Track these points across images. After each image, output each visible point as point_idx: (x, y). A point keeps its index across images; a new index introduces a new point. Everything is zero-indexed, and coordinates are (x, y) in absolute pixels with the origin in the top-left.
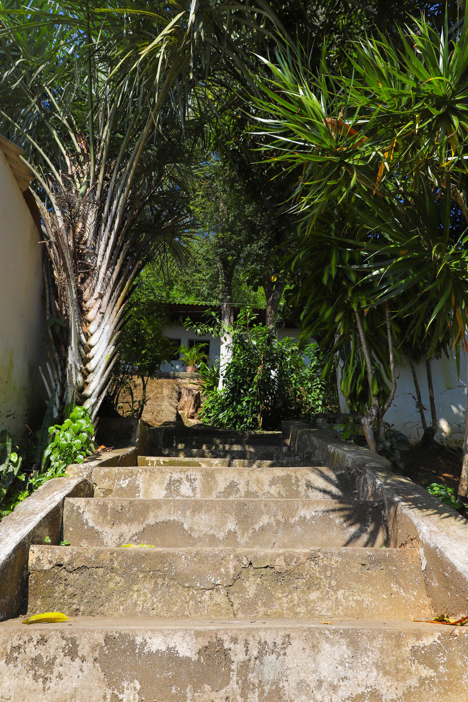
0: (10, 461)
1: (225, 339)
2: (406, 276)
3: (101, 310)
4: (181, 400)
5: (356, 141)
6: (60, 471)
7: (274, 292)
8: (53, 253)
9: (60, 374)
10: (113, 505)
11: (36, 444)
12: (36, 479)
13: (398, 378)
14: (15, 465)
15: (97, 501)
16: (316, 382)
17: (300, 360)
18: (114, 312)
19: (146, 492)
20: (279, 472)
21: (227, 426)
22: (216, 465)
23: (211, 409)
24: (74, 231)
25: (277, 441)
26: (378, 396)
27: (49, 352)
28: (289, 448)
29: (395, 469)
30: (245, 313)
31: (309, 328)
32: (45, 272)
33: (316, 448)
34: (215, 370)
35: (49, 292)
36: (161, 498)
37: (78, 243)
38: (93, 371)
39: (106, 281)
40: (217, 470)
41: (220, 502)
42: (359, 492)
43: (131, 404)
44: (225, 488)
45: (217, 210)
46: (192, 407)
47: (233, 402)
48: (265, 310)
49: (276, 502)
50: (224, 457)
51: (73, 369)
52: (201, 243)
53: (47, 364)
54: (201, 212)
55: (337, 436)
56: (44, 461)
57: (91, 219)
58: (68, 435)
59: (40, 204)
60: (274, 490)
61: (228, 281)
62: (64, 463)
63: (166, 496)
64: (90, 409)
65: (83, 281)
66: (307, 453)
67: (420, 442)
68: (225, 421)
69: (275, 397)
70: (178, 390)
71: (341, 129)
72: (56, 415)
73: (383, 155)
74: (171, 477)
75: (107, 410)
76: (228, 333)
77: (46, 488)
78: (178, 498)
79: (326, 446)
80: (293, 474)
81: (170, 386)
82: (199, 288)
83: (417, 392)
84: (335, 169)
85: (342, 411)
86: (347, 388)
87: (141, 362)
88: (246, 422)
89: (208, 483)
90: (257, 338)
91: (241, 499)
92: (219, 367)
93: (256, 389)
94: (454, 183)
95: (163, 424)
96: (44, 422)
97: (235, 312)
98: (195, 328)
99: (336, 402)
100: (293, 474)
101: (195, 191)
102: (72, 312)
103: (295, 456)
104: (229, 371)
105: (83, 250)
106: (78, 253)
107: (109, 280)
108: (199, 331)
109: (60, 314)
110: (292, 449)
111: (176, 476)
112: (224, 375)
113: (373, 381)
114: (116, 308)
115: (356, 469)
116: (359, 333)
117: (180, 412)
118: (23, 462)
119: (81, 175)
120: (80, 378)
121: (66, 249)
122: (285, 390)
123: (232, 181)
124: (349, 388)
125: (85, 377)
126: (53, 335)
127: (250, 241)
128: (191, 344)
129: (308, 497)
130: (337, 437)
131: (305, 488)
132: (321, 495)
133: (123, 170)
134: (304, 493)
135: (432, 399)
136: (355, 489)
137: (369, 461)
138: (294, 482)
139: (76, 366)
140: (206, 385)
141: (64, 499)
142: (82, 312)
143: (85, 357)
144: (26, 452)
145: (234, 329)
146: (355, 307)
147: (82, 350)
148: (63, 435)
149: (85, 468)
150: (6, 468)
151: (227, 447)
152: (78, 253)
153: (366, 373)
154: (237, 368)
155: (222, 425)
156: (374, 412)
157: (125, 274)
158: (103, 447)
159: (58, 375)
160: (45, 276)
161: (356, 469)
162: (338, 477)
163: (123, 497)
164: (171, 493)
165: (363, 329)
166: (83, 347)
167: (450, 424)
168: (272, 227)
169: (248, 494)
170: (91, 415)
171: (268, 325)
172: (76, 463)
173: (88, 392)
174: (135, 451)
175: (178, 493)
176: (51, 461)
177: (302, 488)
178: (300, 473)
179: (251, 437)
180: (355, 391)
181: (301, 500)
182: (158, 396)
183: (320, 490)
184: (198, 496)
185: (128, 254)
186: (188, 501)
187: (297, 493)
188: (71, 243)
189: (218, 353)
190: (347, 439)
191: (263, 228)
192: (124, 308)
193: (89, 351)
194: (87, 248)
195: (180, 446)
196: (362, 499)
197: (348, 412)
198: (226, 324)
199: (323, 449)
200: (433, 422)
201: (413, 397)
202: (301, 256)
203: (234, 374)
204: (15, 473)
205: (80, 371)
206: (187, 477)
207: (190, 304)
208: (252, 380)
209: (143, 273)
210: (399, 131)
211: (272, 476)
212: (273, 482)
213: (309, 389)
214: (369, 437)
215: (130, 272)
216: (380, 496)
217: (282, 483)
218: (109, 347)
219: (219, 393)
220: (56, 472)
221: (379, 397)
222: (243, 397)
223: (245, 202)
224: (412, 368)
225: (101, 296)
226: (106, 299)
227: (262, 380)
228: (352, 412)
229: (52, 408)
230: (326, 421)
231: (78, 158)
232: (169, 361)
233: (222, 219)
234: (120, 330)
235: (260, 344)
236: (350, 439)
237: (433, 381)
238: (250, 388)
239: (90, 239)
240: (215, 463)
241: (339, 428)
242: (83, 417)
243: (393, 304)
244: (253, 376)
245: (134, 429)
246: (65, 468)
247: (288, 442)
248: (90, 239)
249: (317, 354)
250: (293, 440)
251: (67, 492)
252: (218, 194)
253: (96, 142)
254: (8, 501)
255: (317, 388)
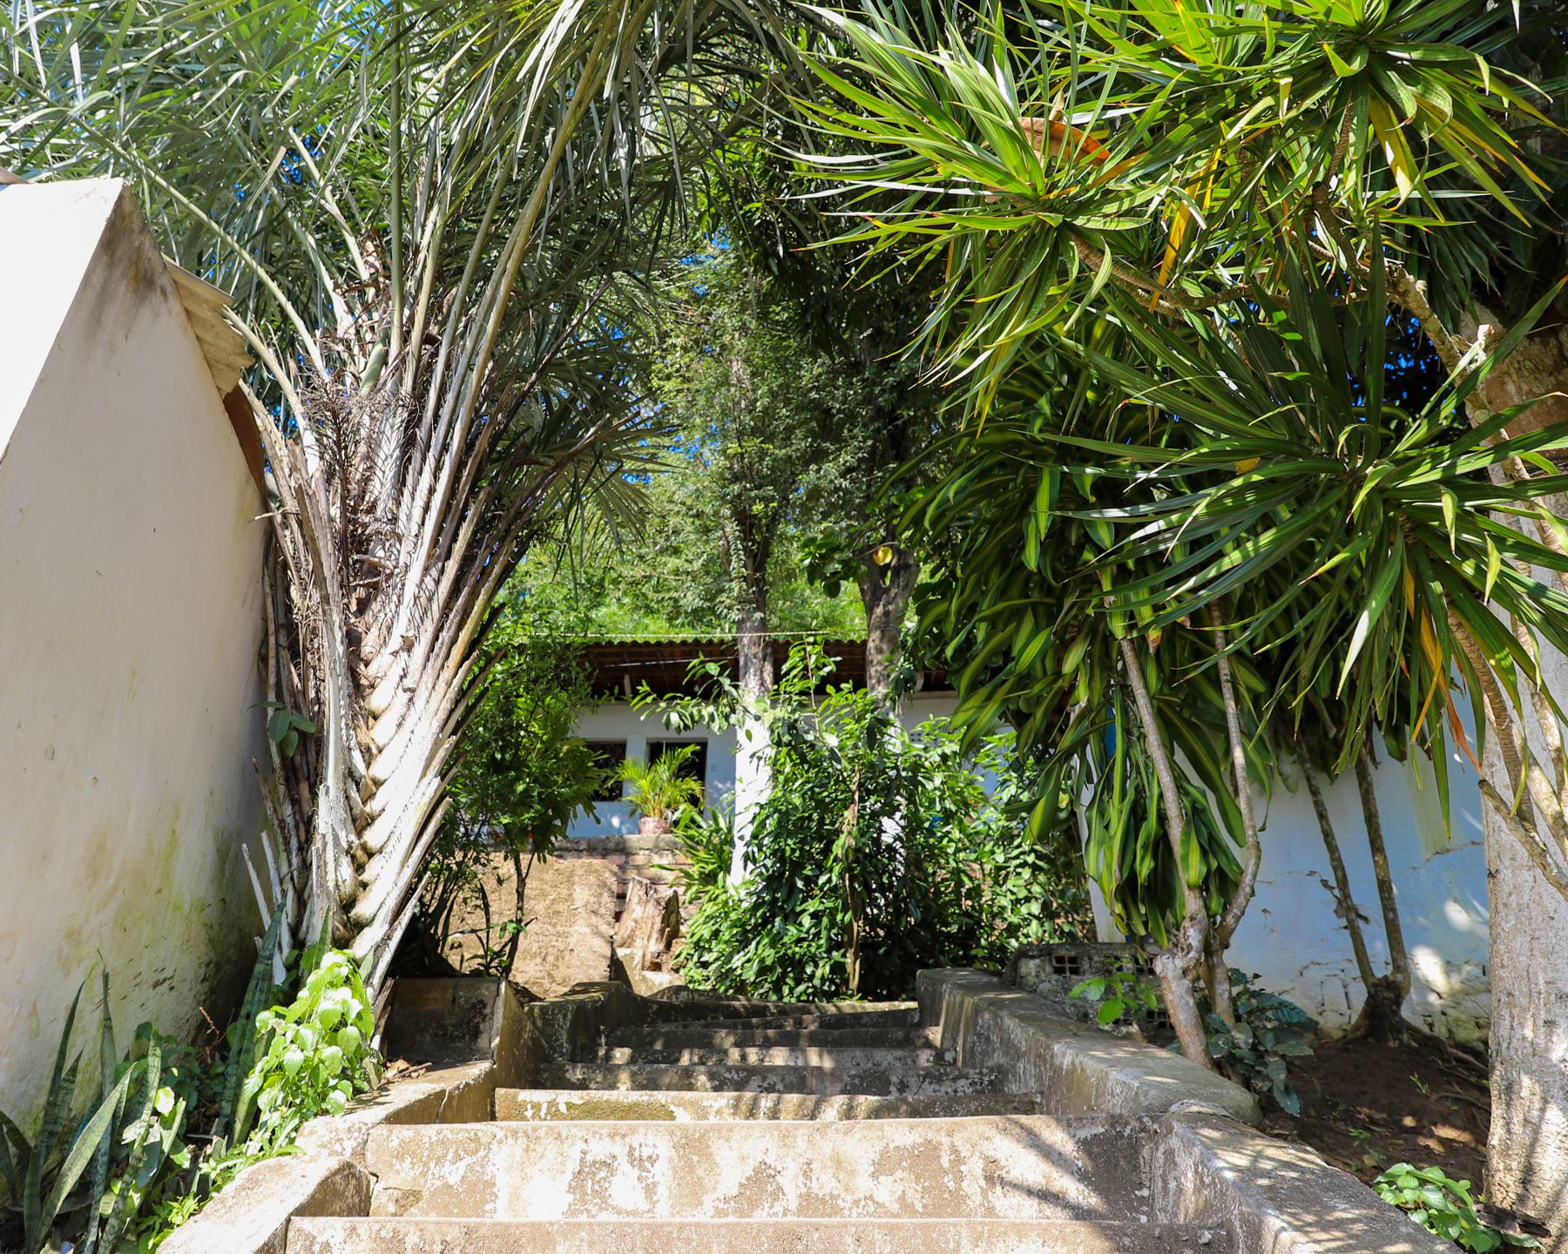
0: (155, 1113)
1: (749, 735)
2: (1267, 522)
3: (408, 683)
4: (624, 916)
5: (1105, 170)
6: (281, 1140)
7: (887, 590)
8: (290, 540)
9: (295, 861)
10: (421, 1237)
11: (224, 1059)
12: (218, 1162)
13: (1263, 829)
14: (166, 1123)
15: (376, 1227)
16: (1019, 846)
17: (971, 783)
18: (441, 686)
19: (515, 1197)
20: (903, 1132)
21: (756, 989)
22: (718, 1112)
23: (709, 941)
24: (345, 481)
25: (904, 1033)
26: (1203, 887)
27: (269, 804)
28: (939, 1055)
29: (1267, 1118)
30: (803, 659)
31: (983, 692)
32: (268, 590)
33: (1019, 1055)
34: (723, 824)
35: (280, 639)
36: (556, 1216)
37: (355, 511)
38: (380, 851)
39: (422, 603)
40: (718, 1129)
41: (723, 1231)
42: (1152, 1196)
43: (483, 935)
44: (741, 1185)
45: (724, 381)
46: (655, 936)
47: (774, 916)
48: (865, 643)
49: (891, 1230)
50: (740, 1086)
51: (330, 847)
52: (682, 476)
53: (264, 836)
54: (679, 391)
55: (1086, 1015)
56: (242, 1109)
57: (390, 447)
58: (308, 1033)
59: (263, 419)
60: (886, 1191)
61: (756, 571)
62: (295, 1113)
63: (571, 1211)
64: (370, 957)
65: (363, 606)
66: (991, 1070)
67: (1356, 1028)
68: (750, 976)
69: (896, 895)
70: (615, 888)
71: (1060, 140)
72: (280, 976)
73: (1176, 198)
74: (584, 1153)
75: (418, 955)
76: (757, 718)
77: (243, 1188)
78: (604, 1217)
79: (1048, 1047)
80: (945, 1140)
81: (592, 879)
82: (675, 595)
83: (1335, 868)
84: (1047, 243)
85: (1102, 936)
86: (1109, 867)
87: (513, 814)
88: (812, 977)
89: (691, 1168)
90: (838, 726)
91: (789, 1218)
92: (733, 813)
93: (841, 876)
94: (1393, 254)
95: (573, 992)
96: (248, 997)
97: (777, 653)
98: (664, 711)
99: (1079, 905)
100: (945, 1140)
101: (663, 336)
102: (333, 691)
103: (955, 1080)
104: (763, 825)
105: (365, 526)
106: (353, 536)
107: (430, 600)
108: (674, 718)
109: (301, 699)
110: (949, 1057)
111: (600, 1149)
112: (748, 838)
113: (1186, 841)
114: (447, 674)
115: (1140, 1119)
116: (1134, 702)
117: (621, 952)
118: (187, 1112)
119: (368, 337)
120: (346, 871)
121: (324, 528)
122: (927, 875)
123: (765, 300)
124: (1115, 867)
125: (359, 868)
126: (284, 760)
127: (818, 456)
128: (655, 751)
129: (990, 1211)
130: (1084, 1017)
131: (983, 1183)
132: (1031, 1205)
133: (473, 310)
134: (978, 1199)
135: (1384, 886)
136: (1141, 1186)
137: (1179, 1096)
138: (946, 1165)
139: (336, 838)
140: (695, 871)
141: (288, 1221)
142: (358, 690)
143: (362, 812)
144: (197, 1083)
145: (773, 706)
146: (1118, 627)
147: (354, 794)
148: (289, 1038)
149: (349, 1130)
150: (142, 1131)
151: (753, 1055)
152: (353, 536)
153: (1162, 818)
154: (785, 816)
155: (741, 987)
156: (1193, 936)
157: (471, 580)
158: (401, 1064)
159: (290, 865)
160: (269, 601)
161: (1140, 1119)
162: (1085, 1145)
163: (450, 1214)
164: (584, 1202)
165: (1146, 687)
166: (357, 784)
167: (1450, 967)
168: (879, 412)
169: (809, 1202)
170: (370, 976)
171: (873, 689)
172: (325, 1112)
173: (362, 909)
174: (490, 1074)
175: (604, 1200)
176: (259, 1111)
177: (973, 1186)
178: (966, 1134)
179: (827, 1023)
180: (1133, 875)
181: (968, 1224)
182: (560, 907)
183: (1030, 1192)
184: (663, 1212)
185: (483, 526)
186: (629, 1225)
187: (955, 1202)
188: (335, 512)
189: (730, 776)
190: (1117, 1022)
191: (851, 417)
192: (470, 669)
193: (372, 796)
194: (376, 520)
195: (621, 1055)
196: (1163, 1219)
197: (1120, 937)
198: (750, 692)
199: (1039, 1056)
200: (1394, 960)
201: (1325, 883)
202: (951, 495)
203: (776, 836)
204: (166, 1147)
205: (347, 852)
206: (631, 1154)
207: (653, 642)
208: (826, 851)
209: (523, 565)
210: (1231, 126)
211: (879, 1146)
212: (882, 1167)
213: (999, 869)
214: (1182, 1015)
215: (485, 572)
216: (1220, 1210)
217: (911, 1168)
218: (426, 780)
219: (732, 891)
220: (271, 1141)
221: (1207, 890)
222: (804, 900)
223: (800, 353)
224: (1315, 792)
225: (408, 646)
226: (420, 650)
227: (857, 850)
228: (1132, 936)
229: (271, 957)
230: (1049, 969)
231: (362, 294)
232: (589, 809)
233: (739, 403)
234: (454, 733)
235: (850, 743)
236: (1128, 1023)
237: (1384, 832)
238: (821, 873)
239: (384, 497)
240: (716, 1105)
241: (1090, 989)
242: (347, 981)
243: (1237, 606)
244: (829, 839)
245: (488, 1011)
246: (296, 1130)
247: (935, 1034)
248: (384, 497)
249: (1018, 766)
250: (951, 1033)
251: (303, 1191)
252: (727, 339)
253: (408, 249)
254: (143, 1227)
255: (1024, 865)
